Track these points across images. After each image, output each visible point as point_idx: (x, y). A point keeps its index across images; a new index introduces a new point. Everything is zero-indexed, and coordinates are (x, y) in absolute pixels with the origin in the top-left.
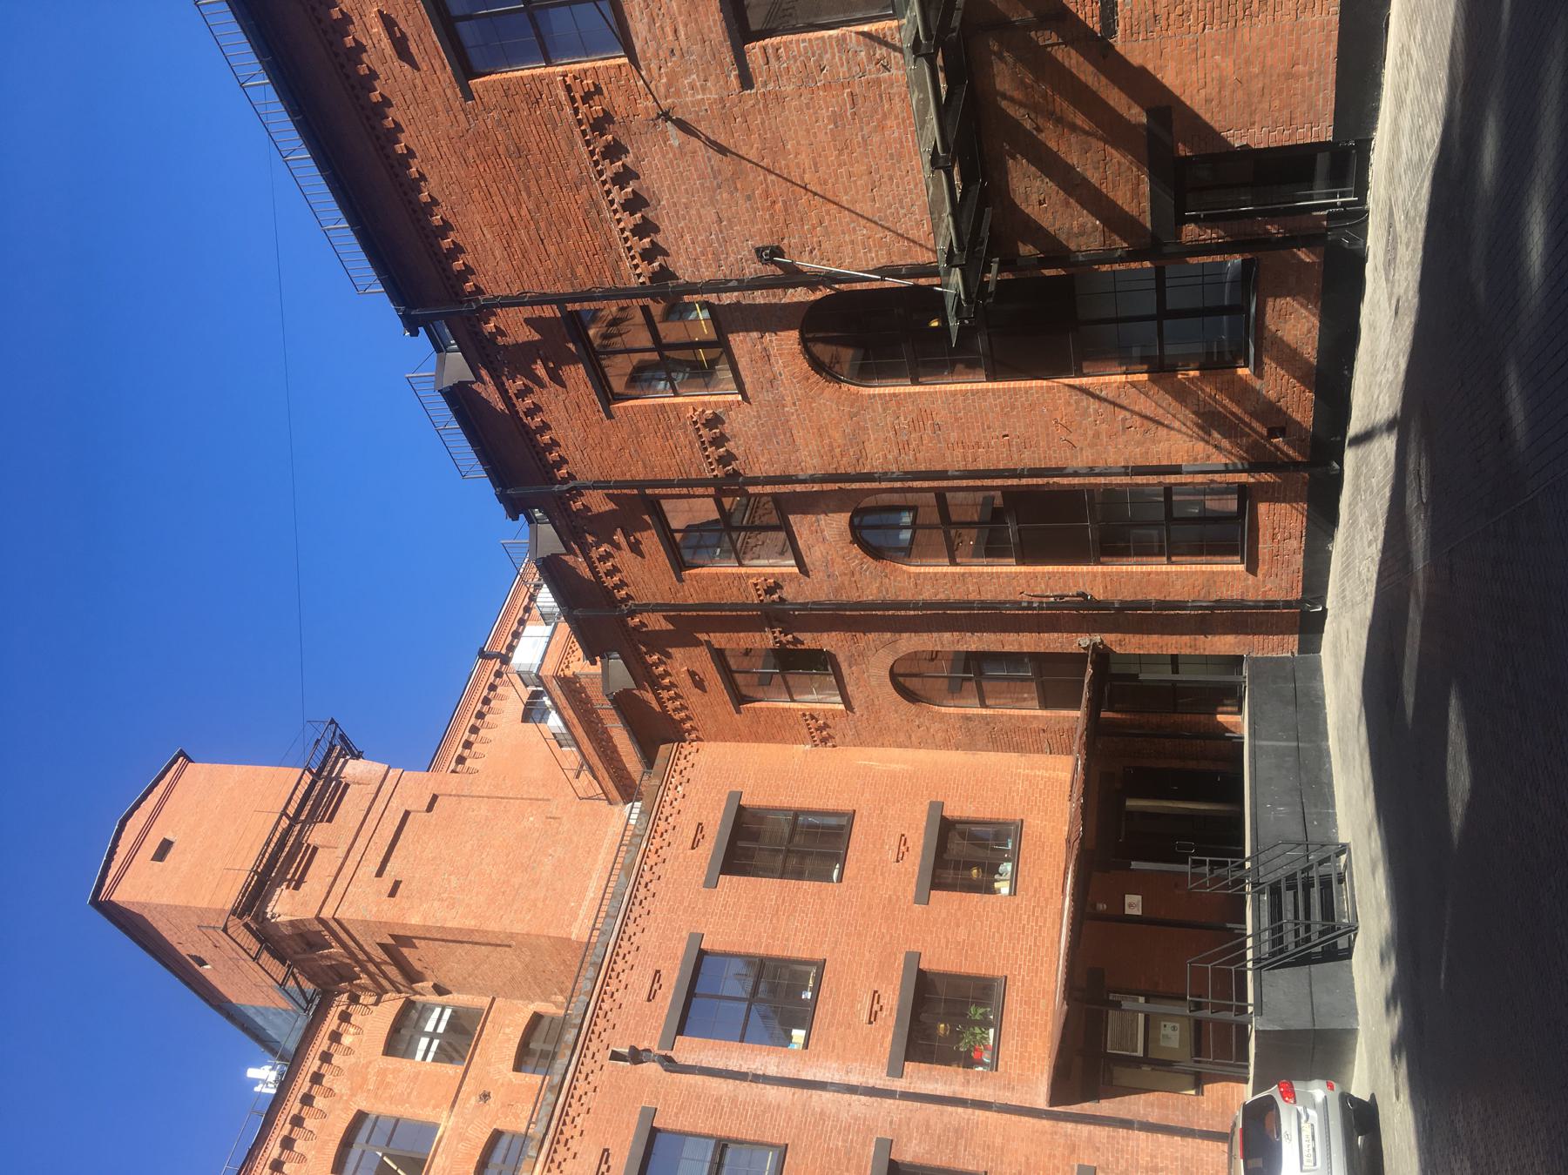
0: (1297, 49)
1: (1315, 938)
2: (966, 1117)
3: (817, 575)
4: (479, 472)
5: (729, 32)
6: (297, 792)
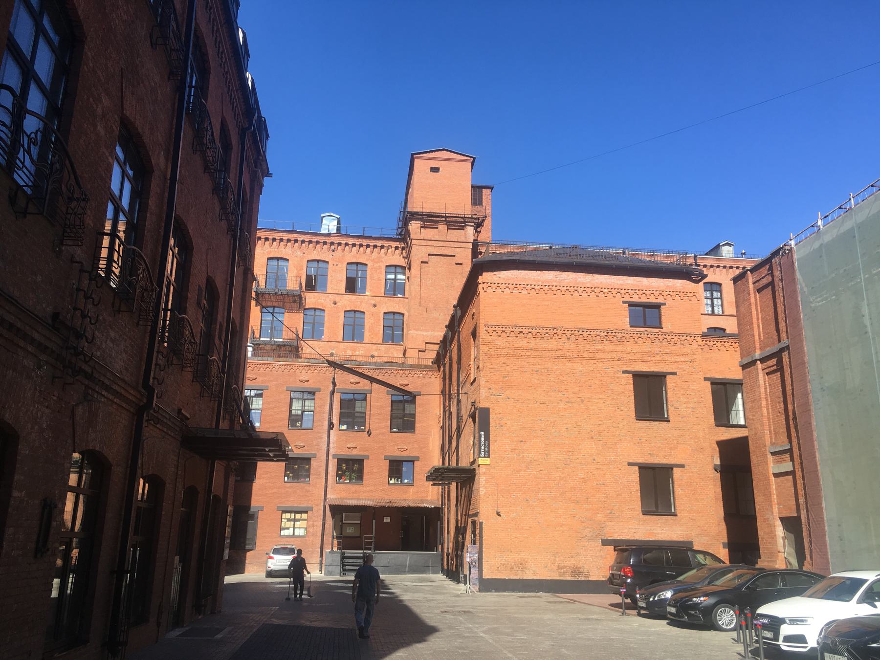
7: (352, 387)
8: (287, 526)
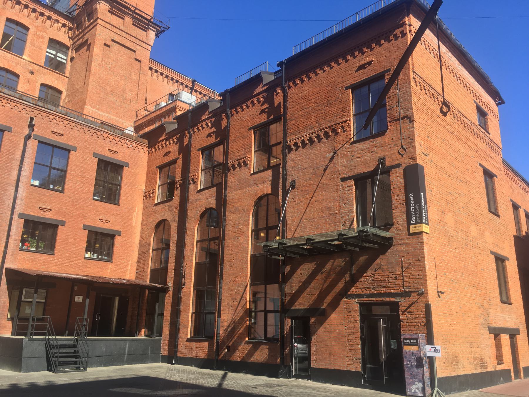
0: (338, 356)
1: (54, 359)
2: (3, 239)
3: (199, 196)
4: (237, 83)
5: (357, 175)
6: (144, 14)
7: (53, 137)
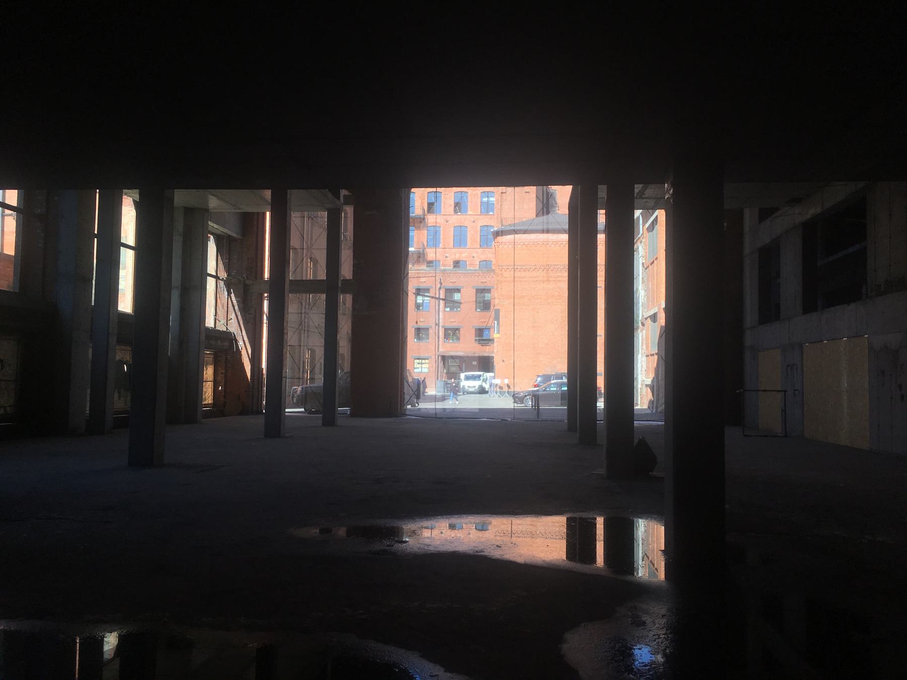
8: (418, 367)
